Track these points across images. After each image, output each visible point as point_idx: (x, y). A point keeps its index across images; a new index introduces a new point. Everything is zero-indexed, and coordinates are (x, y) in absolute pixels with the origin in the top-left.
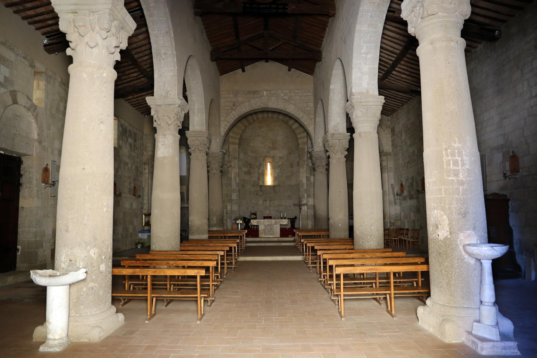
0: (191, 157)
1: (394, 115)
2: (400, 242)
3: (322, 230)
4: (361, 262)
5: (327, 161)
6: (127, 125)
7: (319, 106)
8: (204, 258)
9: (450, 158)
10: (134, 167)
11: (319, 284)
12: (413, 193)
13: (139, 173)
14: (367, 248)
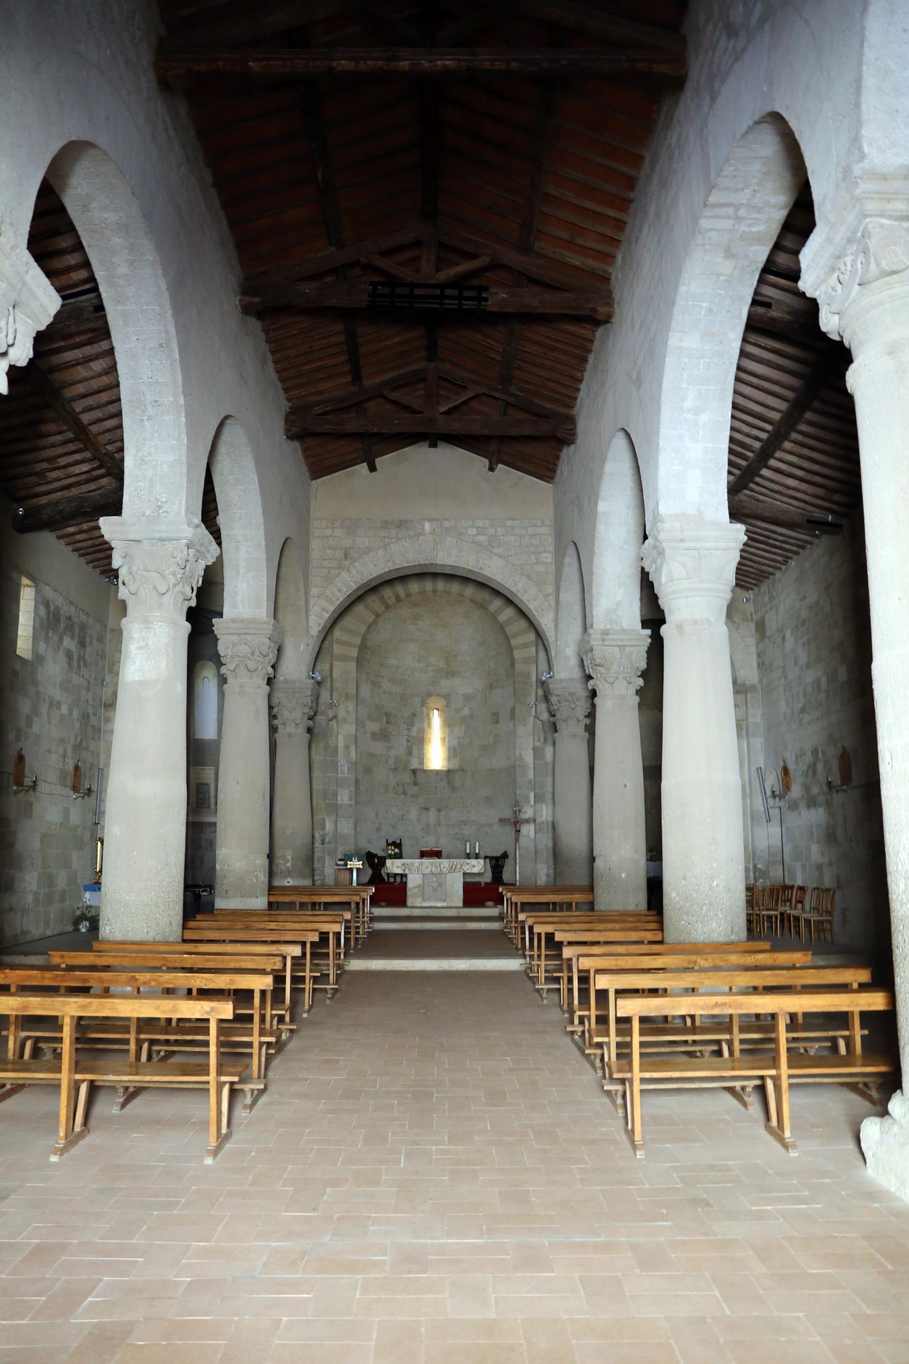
0: (225, 686)
1: (764, 588)
2: (782, 921)
3: (574, 888)
4: (688, 980)
5: (588, 705)
6: (59, 601)
7: (567, 560)
8: (244, 965)
10: (76, 714)
11: (568, 1039)
12: (815, 790)
13: (90, 730)
14: (701, 939)
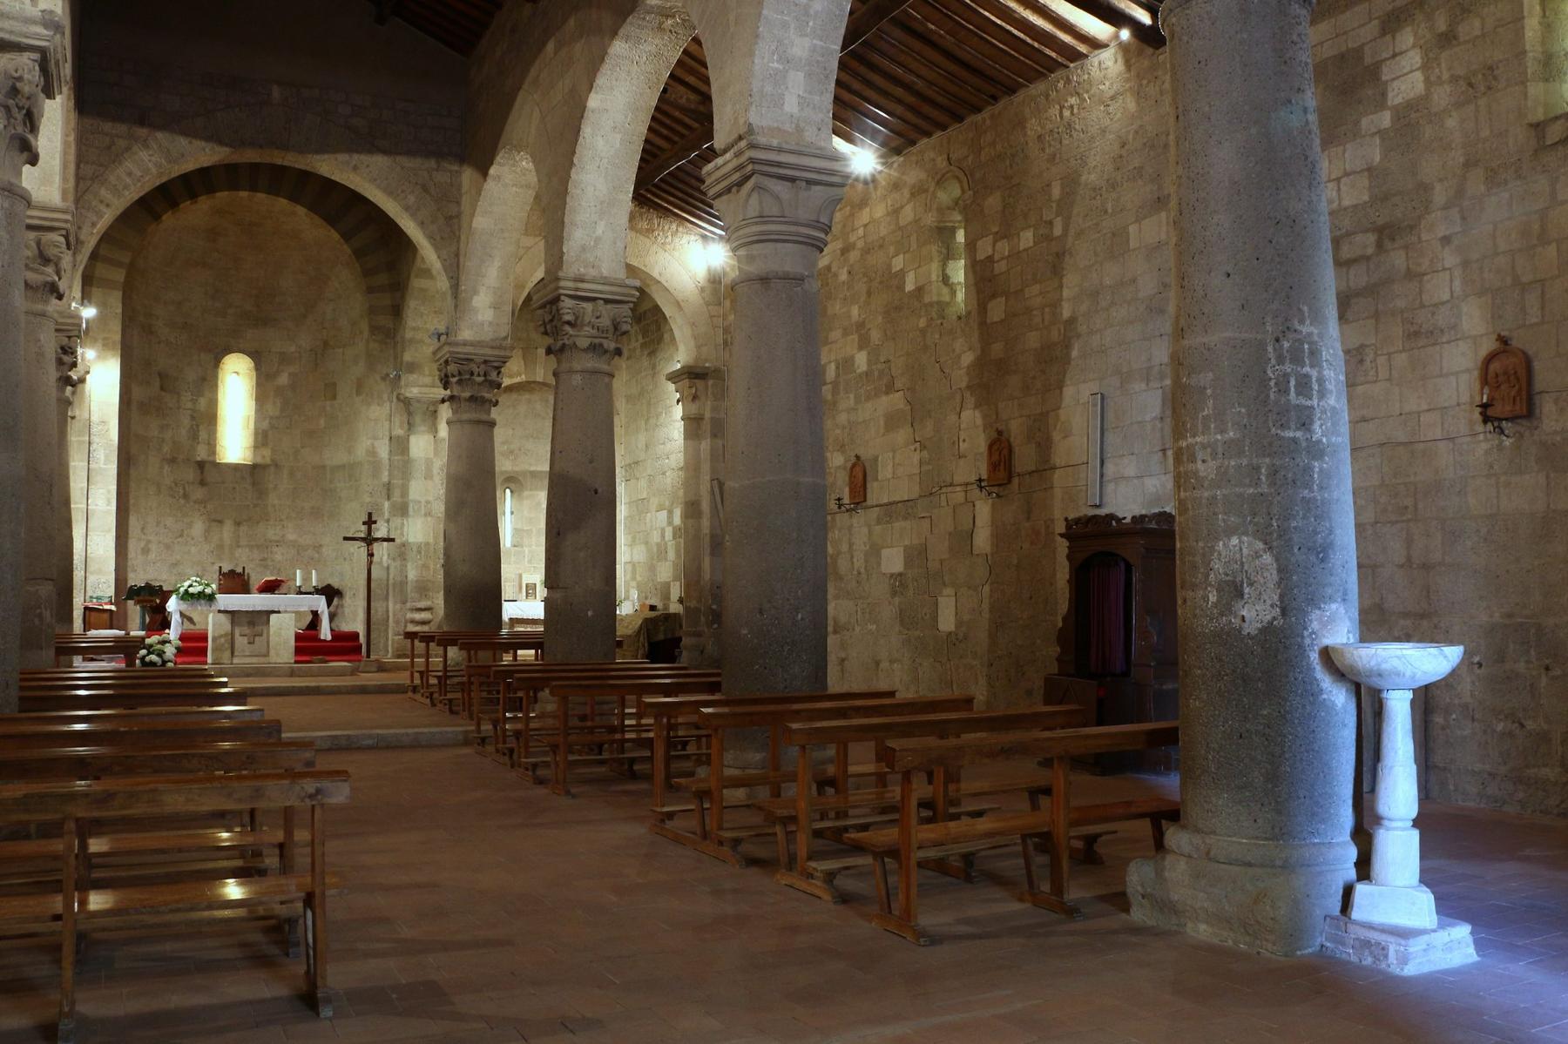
9: (1288, 368)
